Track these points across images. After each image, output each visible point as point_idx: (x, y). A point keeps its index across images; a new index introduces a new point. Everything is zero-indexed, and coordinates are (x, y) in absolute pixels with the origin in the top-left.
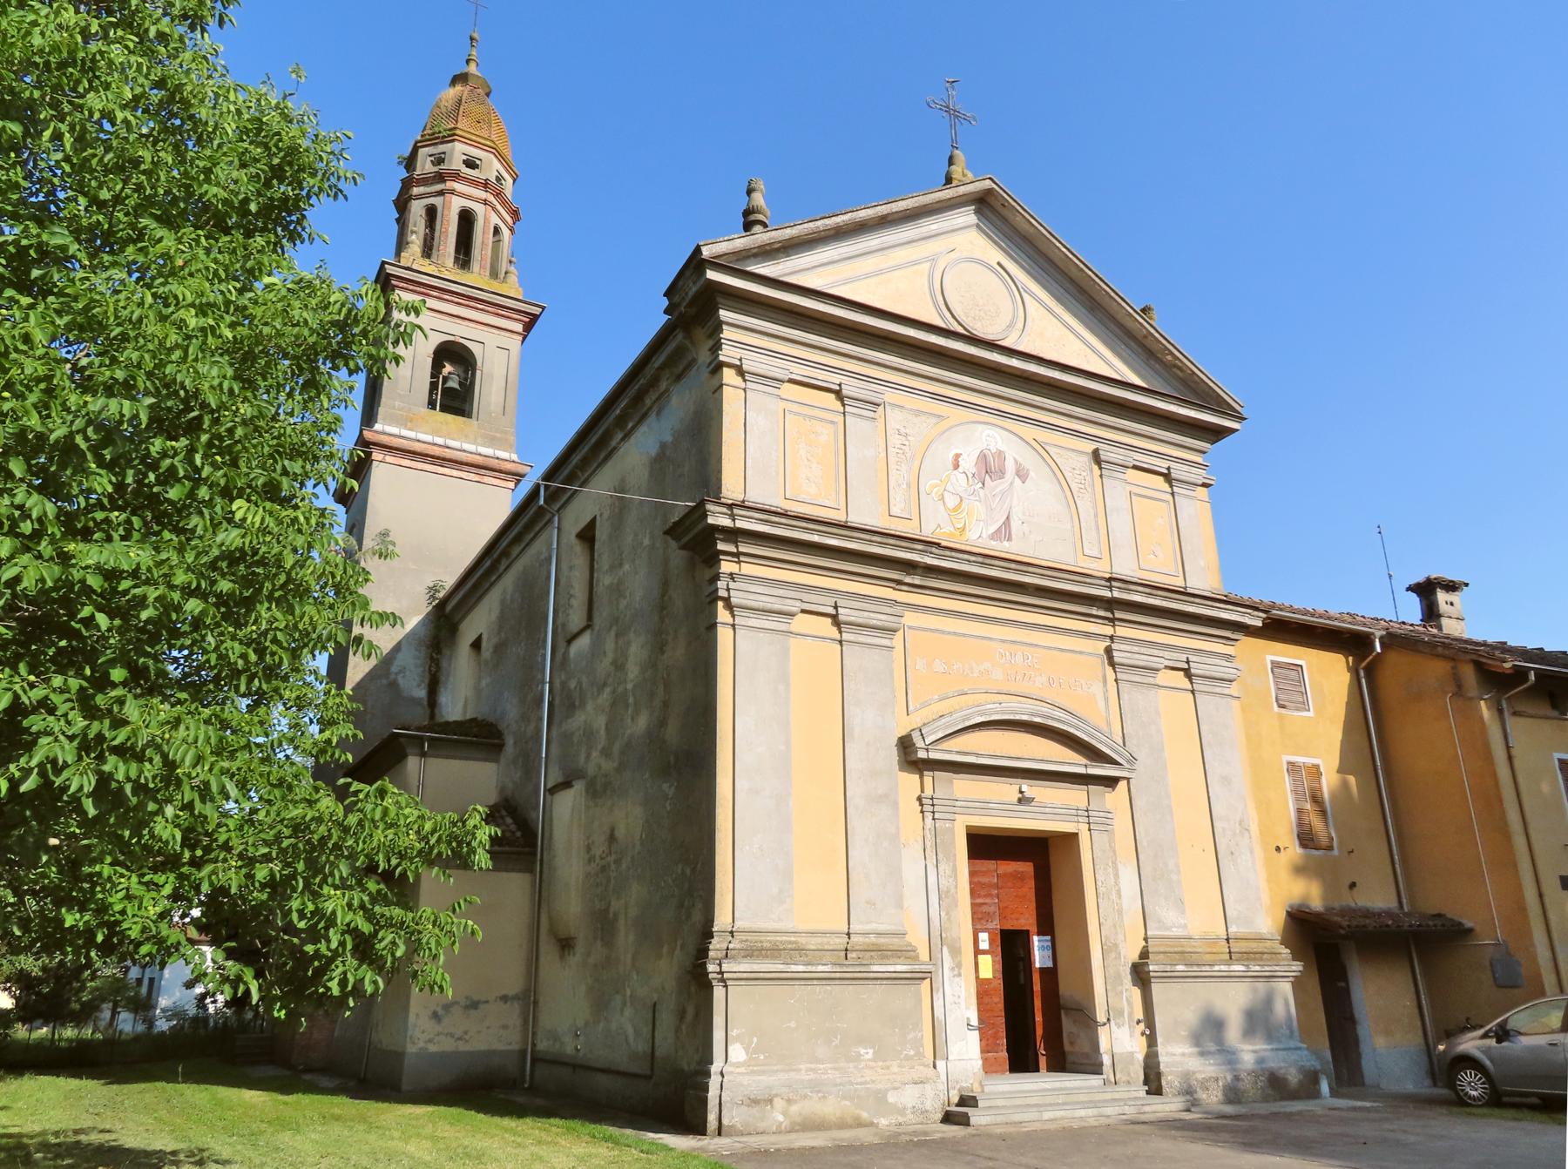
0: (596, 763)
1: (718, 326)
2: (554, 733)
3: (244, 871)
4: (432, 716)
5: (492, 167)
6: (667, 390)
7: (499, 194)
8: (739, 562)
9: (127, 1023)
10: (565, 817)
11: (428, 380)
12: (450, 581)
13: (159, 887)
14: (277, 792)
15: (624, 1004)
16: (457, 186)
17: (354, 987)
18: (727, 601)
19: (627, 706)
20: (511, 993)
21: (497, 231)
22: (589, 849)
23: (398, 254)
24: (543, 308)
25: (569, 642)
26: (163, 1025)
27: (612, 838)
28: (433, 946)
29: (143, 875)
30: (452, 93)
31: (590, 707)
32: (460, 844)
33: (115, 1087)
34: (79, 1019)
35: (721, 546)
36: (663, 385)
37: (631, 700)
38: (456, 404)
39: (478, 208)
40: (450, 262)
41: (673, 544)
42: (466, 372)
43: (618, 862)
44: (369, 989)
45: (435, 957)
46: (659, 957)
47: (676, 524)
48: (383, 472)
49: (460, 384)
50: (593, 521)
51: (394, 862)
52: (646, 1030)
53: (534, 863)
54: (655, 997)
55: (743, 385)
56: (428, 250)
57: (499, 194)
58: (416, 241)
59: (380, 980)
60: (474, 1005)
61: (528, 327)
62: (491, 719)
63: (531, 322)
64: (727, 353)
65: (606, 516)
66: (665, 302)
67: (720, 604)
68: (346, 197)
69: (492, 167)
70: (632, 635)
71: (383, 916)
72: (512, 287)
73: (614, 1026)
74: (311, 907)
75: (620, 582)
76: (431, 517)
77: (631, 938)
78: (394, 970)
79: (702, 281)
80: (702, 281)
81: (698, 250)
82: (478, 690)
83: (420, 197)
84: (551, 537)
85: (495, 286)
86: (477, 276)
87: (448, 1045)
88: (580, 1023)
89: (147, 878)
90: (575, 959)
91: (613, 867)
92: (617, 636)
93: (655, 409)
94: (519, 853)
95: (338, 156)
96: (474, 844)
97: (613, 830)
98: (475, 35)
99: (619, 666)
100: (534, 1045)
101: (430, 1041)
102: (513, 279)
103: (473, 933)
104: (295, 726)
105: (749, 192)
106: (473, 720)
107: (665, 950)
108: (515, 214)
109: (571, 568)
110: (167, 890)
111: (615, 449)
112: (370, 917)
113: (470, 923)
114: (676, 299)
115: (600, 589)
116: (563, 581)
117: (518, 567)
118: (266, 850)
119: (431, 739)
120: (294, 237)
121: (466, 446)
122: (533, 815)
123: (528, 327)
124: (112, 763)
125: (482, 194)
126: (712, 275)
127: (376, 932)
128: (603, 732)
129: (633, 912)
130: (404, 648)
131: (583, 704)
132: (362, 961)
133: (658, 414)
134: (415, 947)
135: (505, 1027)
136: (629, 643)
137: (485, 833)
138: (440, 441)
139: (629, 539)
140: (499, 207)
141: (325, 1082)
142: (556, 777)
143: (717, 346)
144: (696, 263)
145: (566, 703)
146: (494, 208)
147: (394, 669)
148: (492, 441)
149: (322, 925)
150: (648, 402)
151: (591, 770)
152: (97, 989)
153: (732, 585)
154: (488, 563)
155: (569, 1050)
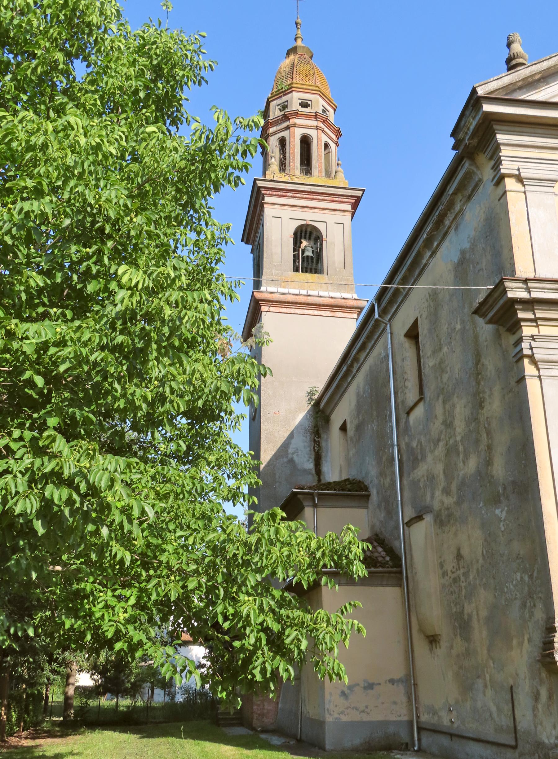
0: (439, 499)
1: (497, 147)
2: (405, 482)
3: (181, 583)
4: (319, 480)
5: (318, 104)
6: (461, 210)
7: (325, 121)
8: (538, 326)
9: (159, 697)
10: (419, 541)
11: (292, 253)
12: (320, 386)
13: (127, 600)
14: (200, 523)
15: (486, 686)
16: (298, 121)
17: (272, 672)
18: (531, 357)
19: (458, 455)
20: (396, 677)
21: (326, 146)
22: (441, 565)
23: (264, 174)
24: (364, 191)
25: (408, 413)
26: (180, 698)
27: (459, 556)
28: (328, 640)
29: (116, 590)
30: (287, 62)
31: (430, 458)
32: (340, 557)
33: (145, 740)
34: (125, 693)
35: (521, 315)
36: (458, 207)
37: (461, 448)
38: (313, 266)
39: (313, 133)
40: (298, 171)
41: (480, 321)
42: (316, 244)
43: (466, 574)
44: (285, 676)
45: (331, 650)
46: (510, 648)
47: (482, 304)
48: (269, 319)
49: (313, 252)
50: (416, 322)
51: (291, 573)
52: (507, 708)
53: (402, 579)
54: (511, 682)
55: (523, 189)
56: (283, 167)
57: (325, 121)
58: (274, 163)
59: (291, 669)
60: (370, 686)
61: (355, 206)
62: (359, 478)
63: (356, 203)
64: (507, 167)
65: (424, 316)
66: (452, 141)
67: (526, 361)
68: (207, 82)
69: (318, 104)
70: (455, 399)
71: (288, 617)
72: (341, 180)
73: (479, 704)
74: (231, 610)
75: (442, 362)
76: (305, 346)
77: (485, 633)
78: (303, 660)
79: (481, 113)
80: (481, 113)
81: (474, 91)
82: (348, 460)
83: (275, 133)
84: (386, 341)
85: (330, 182)
86: (317, 177)
87: (356, 717)
88: (452, 702)
89: (117, 593)
90: (441, 651)
91: (462, 578)
92: (444, 402)
93: (453, 226)
94: (390, 573)
95: (197, 52)
96: (351, 556)
97: (459, 550)
98: (299, 21)
99: (448, 424)
100: (418, 717)
101: (342, 713)
102: (341, 175)
103: (359, 630)
104: (215, 479)
105: (509, 45)
106: (346, 480)
107: (515, 642)
108: (338, 133)
109: (403, 360)
110: (132, 601)
111: (426, 265)
112: (279, 619)
113: (356, 622)
114: (461, 135)
115: (426, 371)
116: (399, 371)
117: (366, 367)
118: (195, 567)
119: (319, 495)
120: (175, 122)
121: (322, 293)
122: (396, 543)
123: (355, 206)
124: (50, 490)
125: (314, 123)
126: (487, 108)
127: (284, 630)
128: (442, 476)
129: (484, 613)
130: (295, 435)
131: (424, 457)
132: (276, 653)
133: (456, 229)
134: (314, 643)
135: (395, 703)
136: (454, 406)
137: (357, 550)
138: (304, 292)
139: (445, 328)
140: (326, 129)
141: (276, 740)
142: (410, 513)
143: (498, 162)
144: (474, 101)
145: (412, 459)
146: (323, 131)
147: (290, 451)
148: (339, 286)
149: (240, 625)
150: (447, 223)
151: (436, 506)
152: (139, 674)
153: (534, 344)
154: (344, 369)
155: (446, 722)
